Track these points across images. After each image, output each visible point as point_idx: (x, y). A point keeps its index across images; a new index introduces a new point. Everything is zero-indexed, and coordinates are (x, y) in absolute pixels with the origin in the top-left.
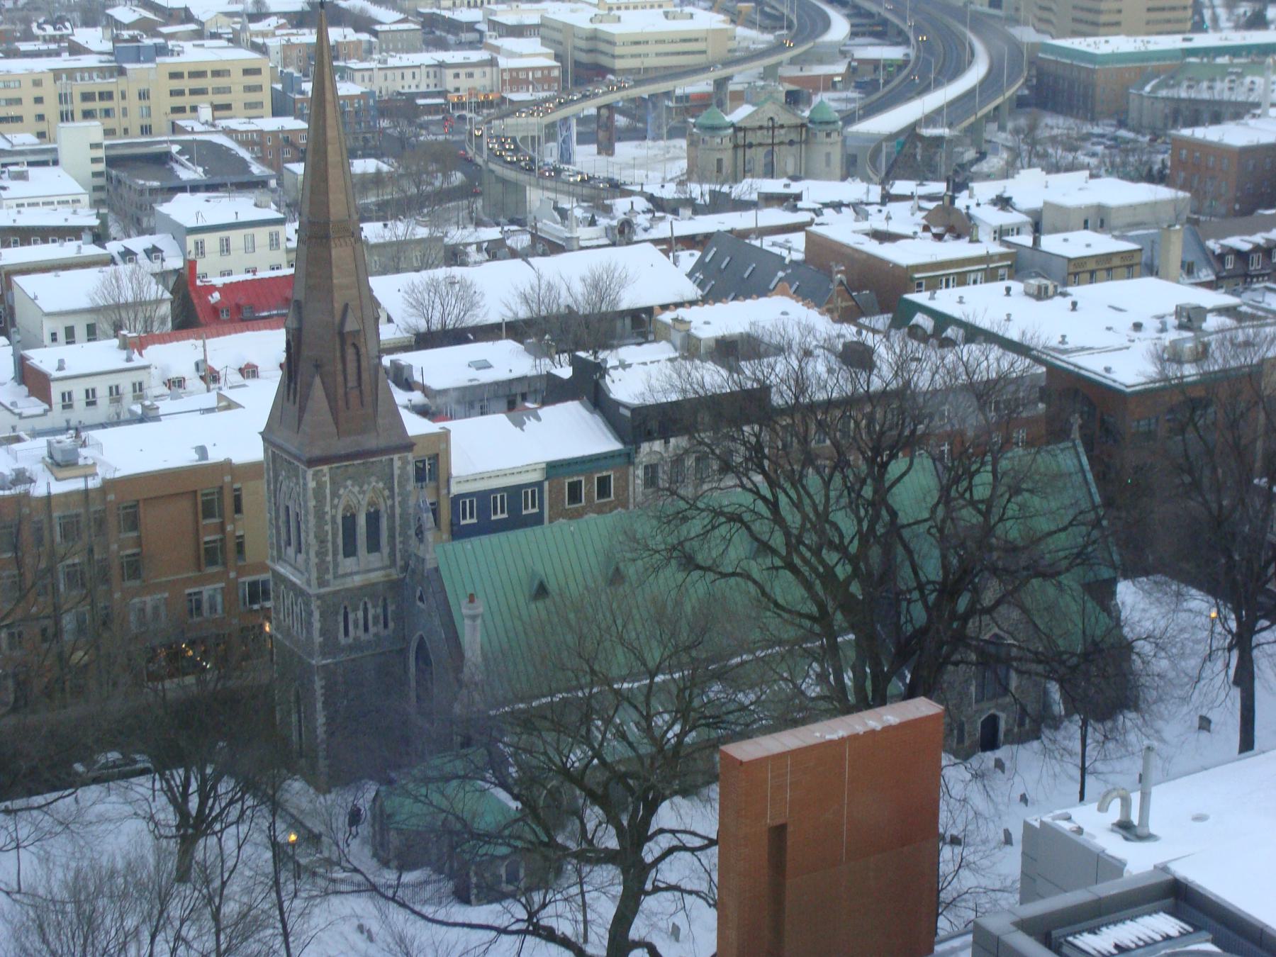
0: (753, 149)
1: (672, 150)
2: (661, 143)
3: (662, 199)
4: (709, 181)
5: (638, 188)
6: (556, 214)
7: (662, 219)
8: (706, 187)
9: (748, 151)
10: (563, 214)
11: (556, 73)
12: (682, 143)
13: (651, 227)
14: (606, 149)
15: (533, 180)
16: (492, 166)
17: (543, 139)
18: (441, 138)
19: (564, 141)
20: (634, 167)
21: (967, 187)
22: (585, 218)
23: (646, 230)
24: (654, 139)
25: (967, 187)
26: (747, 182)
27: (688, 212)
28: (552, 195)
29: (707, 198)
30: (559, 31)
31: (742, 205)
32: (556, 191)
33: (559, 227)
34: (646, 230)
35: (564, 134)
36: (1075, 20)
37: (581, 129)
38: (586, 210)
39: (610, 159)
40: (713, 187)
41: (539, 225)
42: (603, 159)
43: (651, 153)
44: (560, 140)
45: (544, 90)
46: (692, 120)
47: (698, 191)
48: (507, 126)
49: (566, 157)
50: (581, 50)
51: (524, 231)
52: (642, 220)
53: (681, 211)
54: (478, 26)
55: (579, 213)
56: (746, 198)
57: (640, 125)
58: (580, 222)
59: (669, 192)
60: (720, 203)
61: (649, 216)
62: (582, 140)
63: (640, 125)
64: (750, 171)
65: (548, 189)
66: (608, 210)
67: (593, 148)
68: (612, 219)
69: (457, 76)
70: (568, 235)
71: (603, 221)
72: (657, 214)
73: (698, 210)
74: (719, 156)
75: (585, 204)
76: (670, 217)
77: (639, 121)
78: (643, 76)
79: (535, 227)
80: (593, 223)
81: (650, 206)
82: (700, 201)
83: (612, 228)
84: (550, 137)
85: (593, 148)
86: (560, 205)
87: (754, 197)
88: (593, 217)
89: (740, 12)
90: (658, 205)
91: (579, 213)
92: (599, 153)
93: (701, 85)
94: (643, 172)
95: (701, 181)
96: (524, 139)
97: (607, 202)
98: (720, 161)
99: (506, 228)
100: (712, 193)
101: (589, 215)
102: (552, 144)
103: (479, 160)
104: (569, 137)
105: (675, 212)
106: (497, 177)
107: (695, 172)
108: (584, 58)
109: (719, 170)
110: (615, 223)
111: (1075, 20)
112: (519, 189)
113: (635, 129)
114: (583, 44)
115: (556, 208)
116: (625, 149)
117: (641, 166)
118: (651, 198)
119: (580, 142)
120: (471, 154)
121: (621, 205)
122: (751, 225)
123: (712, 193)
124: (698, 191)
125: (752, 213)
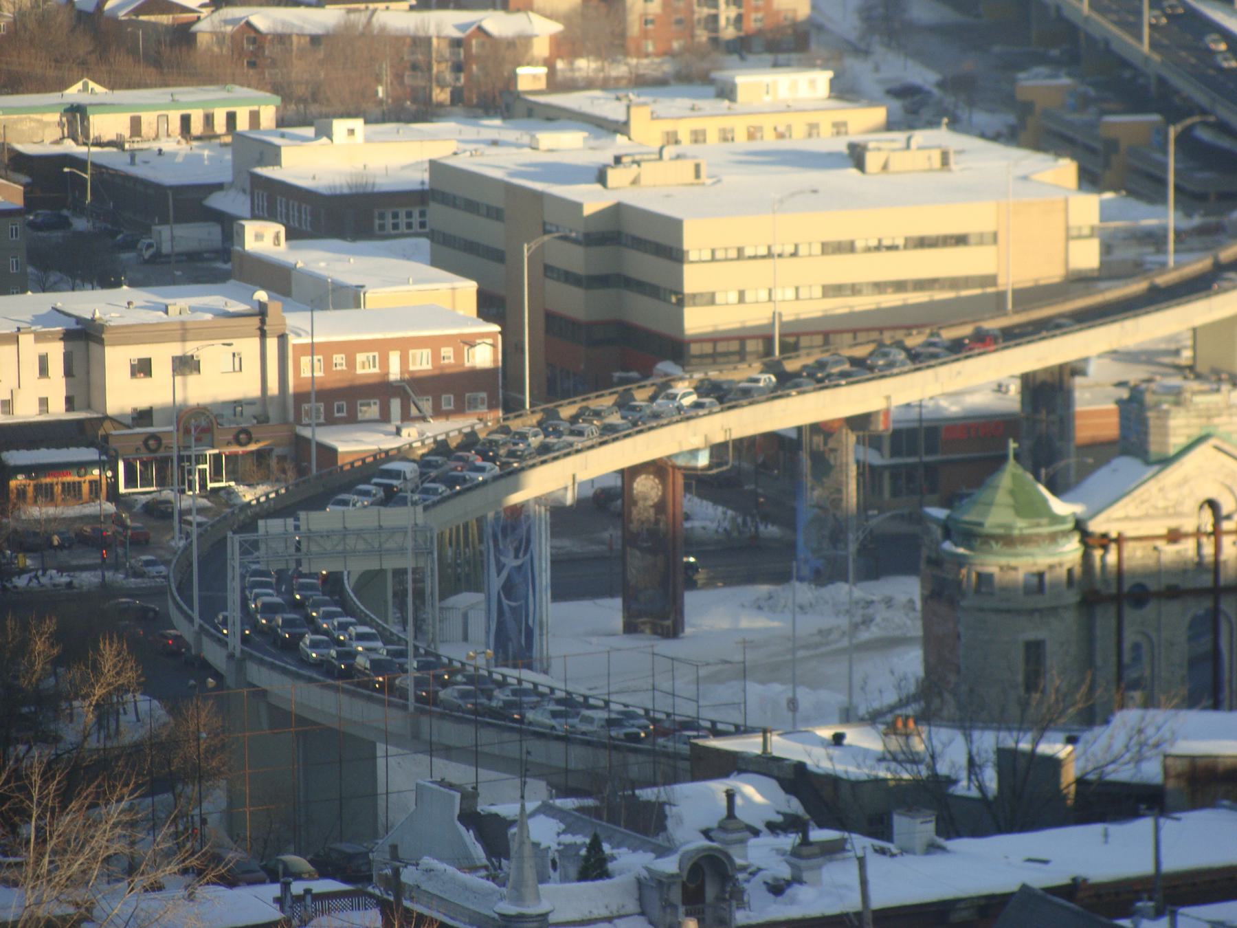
0: (1150, 610)
1: (881, 614)
2: (841, 591)
3: (834, 781)
4: (999, 722)
5: (750, 745)
6: (469, 837)
7: (832, 850)
8: (987, 741)
9: (1130, 615)
10: (494, 835)
11: (483, 357)
12: (908, 589)
13: (797, 880)
14: (656, 613)
15: (395, 720)
16: (260, 676)
17: (432, 585)
18: (88, 579)
19: (508, 589)
20: (744, 673)
21: (172, 789)
22: (567, 851)
23: (777, 889)
24: (820, 578)
25: (172, 789)
26: (1127, 719)
27: (923, 828)
28: (460, 773)
29: (990, 778)
30: (495, 214)
31: (1107, 802)
32: (476, 757)
33: (476, 880)
34: (777, 889)
35: (510, 562)
36: (458, 528)
37: (569, 545)
38: (570, 822)
39: (666, 647)
40: (1008, 740)
41: (408, 876)
42: (643, 649)
43: (809, 625)
44: (496, 582)
45: (438, 413)
46: (940, 513)
47: (952, 751)
48: (310, 536)
49: (515, 640)
50: (569, 278)
51: (357, 898)
52: (764, 855)
53: (900, 823)
54: (217, 201)
55: (545, 832)
56: (1122, 773)
57: (771, 530)
58: (549, 865)
59: (857, 752)
60: (1030, 797)
61: (789, 841)
62: (573, 582)
63: (771, 530)
64: (1136, 685)
65: (448, 752)
66: (648, 824)
67: (610, 611)
68: (662, 852)
69: (143, 368)
70: (511, 909)
71: (630, 861)
72: (818, 835)
73: (959, 817)
74: (1032, 635)
75: (569, 803)
76: (860, 843)
77: (766, 518)
78: (789, 355)
79: (394, 883)
80: (593, 867)
81: (795, 806)
82: (963, 788)
83: (661, 883)
84: (462, 575)
85: (610, 611)
86: (483, 807)
87: (1151, 771)
88: (595, 846)
89: (1112, 146)
90: (824, 804)
91: (545, 832)
92: (630, 628)
93: (979, 383)
94: (780, 691)
95: (966, 723)
96: (370, 580)
97: (647, 794)
98: (1035, 650)
99: (297, 888)
100: (1007, 759)
101: (582, 839)
102: (465, 599)
103: (215, 655)
104: (525, 573)
105: (879, 828)
106: (272, 708)
107: (938, 697)
108: (574, 303)
109: (1033, 681)
110: (669, 865)
111: (458, 528)
112: (350, 755)
113: (755, 545)
114: (575, 259)
115: (470, 818)
116: (719, 616)
117: (771, 672)
118: (796, 779)
119: (560, 594)
120: (184, 629)
121: (695, 805)
122: (1142, 866)
123: (1007, 759)
124: (952, 751)
125: (1144, 826)
